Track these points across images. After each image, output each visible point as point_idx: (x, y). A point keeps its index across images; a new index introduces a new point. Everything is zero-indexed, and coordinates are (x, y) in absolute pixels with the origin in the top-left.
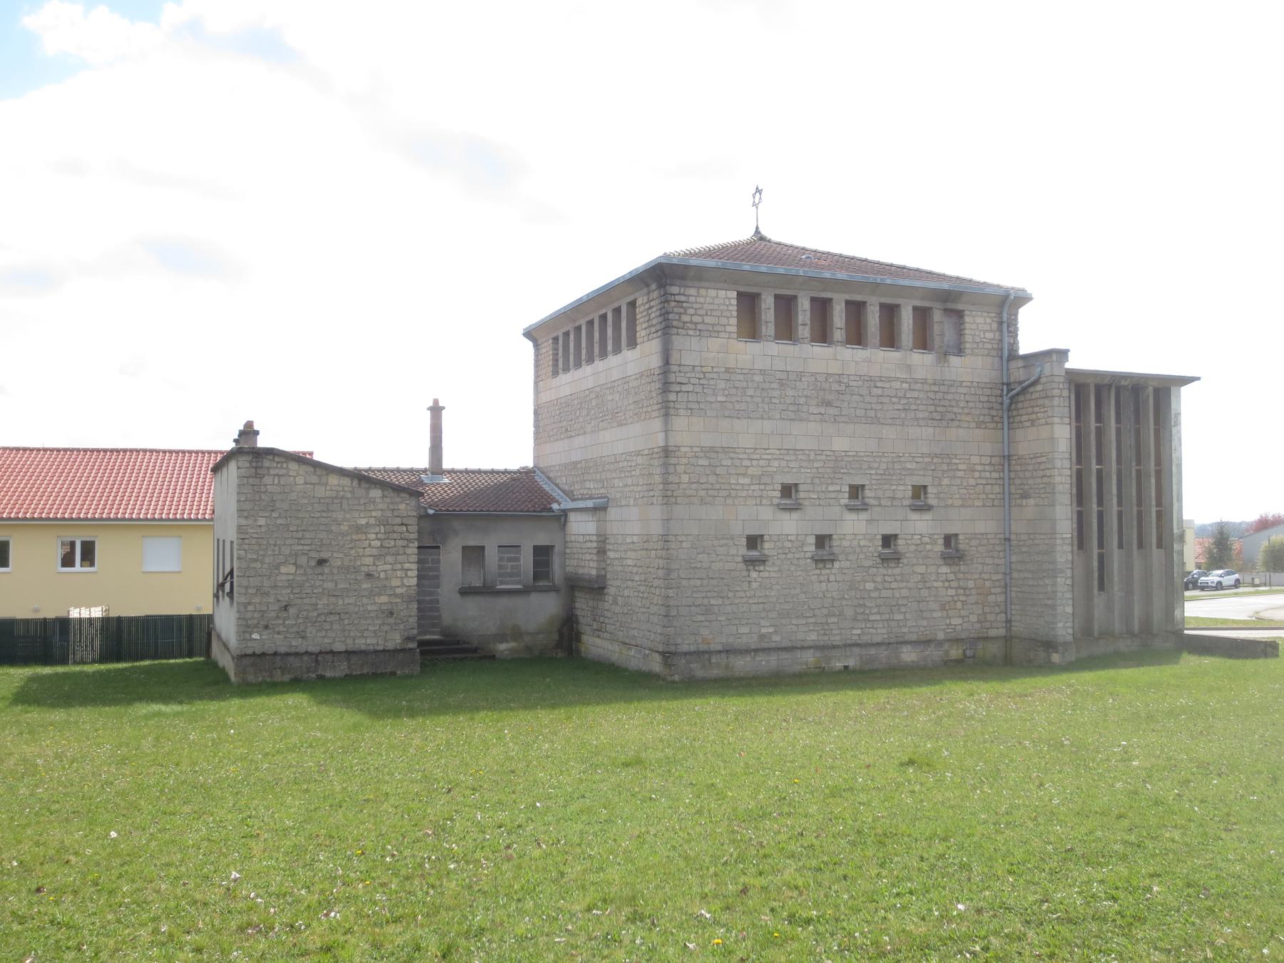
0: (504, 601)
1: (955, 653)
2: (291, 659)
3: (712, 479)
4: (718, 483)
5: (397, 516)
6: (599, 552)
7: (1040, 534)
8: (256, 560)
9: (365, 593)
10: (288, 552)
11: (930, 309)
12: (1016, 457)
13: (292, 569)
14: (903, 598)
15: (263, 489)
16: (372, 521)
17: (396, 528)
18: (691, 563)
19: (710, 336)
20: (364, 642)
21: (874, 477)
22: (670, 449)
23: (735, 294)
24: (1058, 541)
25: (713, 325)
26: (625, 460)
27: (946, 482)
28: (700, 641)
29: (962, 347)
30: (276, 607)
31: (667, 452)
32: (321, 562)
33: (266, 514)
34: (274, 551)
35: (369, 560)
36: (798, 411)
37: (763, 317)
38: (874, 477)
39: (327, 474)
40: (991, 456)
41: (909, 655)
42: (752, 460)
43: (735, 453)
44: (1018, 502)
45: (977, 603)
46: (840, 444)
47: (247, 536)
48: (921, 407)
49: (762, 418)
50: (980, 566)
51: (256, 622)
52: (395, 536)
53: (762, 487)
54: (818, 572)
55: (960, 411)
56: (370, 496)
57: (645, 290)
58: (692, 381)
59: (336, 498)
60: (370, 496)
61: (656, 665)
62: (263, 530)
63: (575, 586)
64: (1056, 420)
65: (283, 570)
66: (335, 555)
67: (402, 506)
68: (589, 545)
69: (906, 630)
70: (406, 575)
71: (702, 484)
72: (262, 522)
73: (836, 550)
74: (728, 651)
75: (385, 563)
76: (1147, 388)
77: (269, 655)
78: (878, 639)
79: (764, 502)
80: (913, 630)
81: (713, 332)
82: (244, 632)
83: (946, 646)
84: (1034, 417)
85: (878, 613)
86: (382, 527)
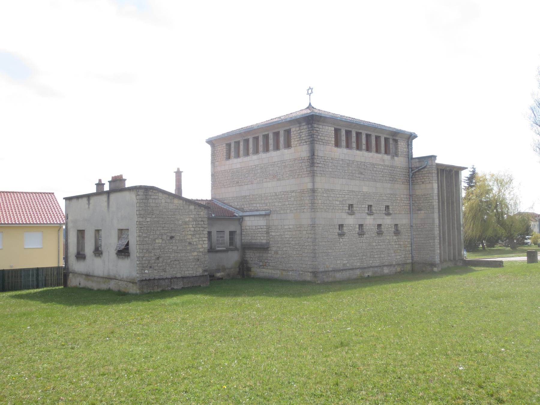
0: (219, 255)
1: (399, 269)
2: (161, 281)
3: (328, 202)
4: (330, 203)
5: (200, 217)
6: (267, 233)
7: (427, 224)
8: (146, 237)
9: (189, 251)
10: (159, 233)
11: (389, 138)
12: (415, 195)
13: (160, 241)
14: (383, 248)
15: (149, 205)
16: (191, 219)
17: (200, 223)
18: (322, 236)
19: (327, 145)
20: (188, 273)
21: (375, 202)
22: (316, 189)
23: (333, 129)
24: (435, 226)
25: (327, 140)
26: (283, 194)
27: (394, 204)
28: (325, 267)
29: (397, 153)
30: (154, 258)
31: (313, 191)
32: (172, 238)
33: (151, 216)
34: (153, 233)
35: (190, 237)
36: (353, 176)
37: (342, 139)
38: (375, 202)
39: (174, 199)
40: (407, 195)
41: (386, 271)
42: (340, 194)
43: (335, 192)
44: (416, 212)
45: (404, 250)
46: (365, 189)
47: (143, 226)
48: (387, 176)
49: (342, 178)
50: (404, 236)
51: (146, 265)
52: (200, 226)
53: (343, 205)
54: (359, 239)
55: (398, 178)
56: (190, 208)
57: (298, 125)
58: (322, 162)
59: (177, 209)
60: (190, 208)
61: (308, 277)
62: (149, 223)
63: (247, 247)
64: (434, 182)
65: (157, 241)
66: (177, 234)
67: (202, 213)
68: (263, 230)
69: (384, 261)
70: (204, 243)
71: (325, 204)
72: (148, 220)
73: (365, 230)
74: (335, 271)
75: (196, 238)
76: (452, 171)
77: (152, 280)
78: (377, 265)
79: (343, 211)
80: (387, 261)
81: (328, 144)
82: (142, 270)
83: (396, 267)
84: (423, 180)
85: (377, 255)
86: (194, 222)
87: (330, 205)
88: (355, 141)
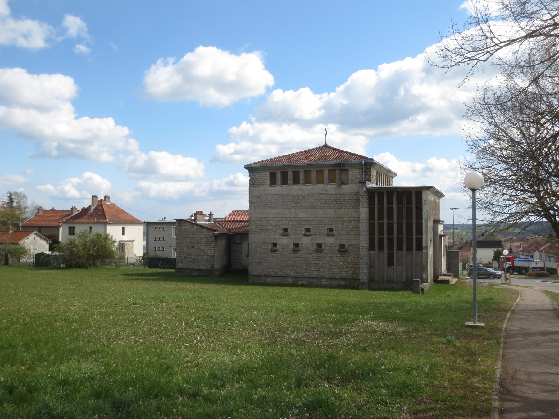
3: (261, 227)
17: (209, 239)
23: (268, 173)
32: (193, 247)
46: (301, 215)
53: (276, 229)
67: (210, 233)
74: (266, 276)
78: (315, 276)
81: (262, 185)
87: (263, 229)
88: (291, 179)
